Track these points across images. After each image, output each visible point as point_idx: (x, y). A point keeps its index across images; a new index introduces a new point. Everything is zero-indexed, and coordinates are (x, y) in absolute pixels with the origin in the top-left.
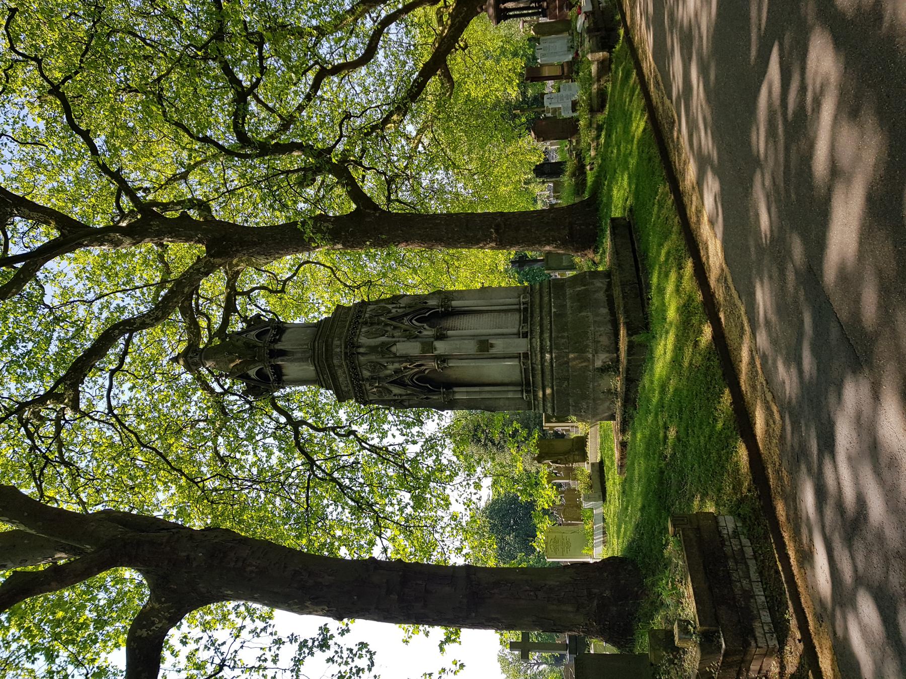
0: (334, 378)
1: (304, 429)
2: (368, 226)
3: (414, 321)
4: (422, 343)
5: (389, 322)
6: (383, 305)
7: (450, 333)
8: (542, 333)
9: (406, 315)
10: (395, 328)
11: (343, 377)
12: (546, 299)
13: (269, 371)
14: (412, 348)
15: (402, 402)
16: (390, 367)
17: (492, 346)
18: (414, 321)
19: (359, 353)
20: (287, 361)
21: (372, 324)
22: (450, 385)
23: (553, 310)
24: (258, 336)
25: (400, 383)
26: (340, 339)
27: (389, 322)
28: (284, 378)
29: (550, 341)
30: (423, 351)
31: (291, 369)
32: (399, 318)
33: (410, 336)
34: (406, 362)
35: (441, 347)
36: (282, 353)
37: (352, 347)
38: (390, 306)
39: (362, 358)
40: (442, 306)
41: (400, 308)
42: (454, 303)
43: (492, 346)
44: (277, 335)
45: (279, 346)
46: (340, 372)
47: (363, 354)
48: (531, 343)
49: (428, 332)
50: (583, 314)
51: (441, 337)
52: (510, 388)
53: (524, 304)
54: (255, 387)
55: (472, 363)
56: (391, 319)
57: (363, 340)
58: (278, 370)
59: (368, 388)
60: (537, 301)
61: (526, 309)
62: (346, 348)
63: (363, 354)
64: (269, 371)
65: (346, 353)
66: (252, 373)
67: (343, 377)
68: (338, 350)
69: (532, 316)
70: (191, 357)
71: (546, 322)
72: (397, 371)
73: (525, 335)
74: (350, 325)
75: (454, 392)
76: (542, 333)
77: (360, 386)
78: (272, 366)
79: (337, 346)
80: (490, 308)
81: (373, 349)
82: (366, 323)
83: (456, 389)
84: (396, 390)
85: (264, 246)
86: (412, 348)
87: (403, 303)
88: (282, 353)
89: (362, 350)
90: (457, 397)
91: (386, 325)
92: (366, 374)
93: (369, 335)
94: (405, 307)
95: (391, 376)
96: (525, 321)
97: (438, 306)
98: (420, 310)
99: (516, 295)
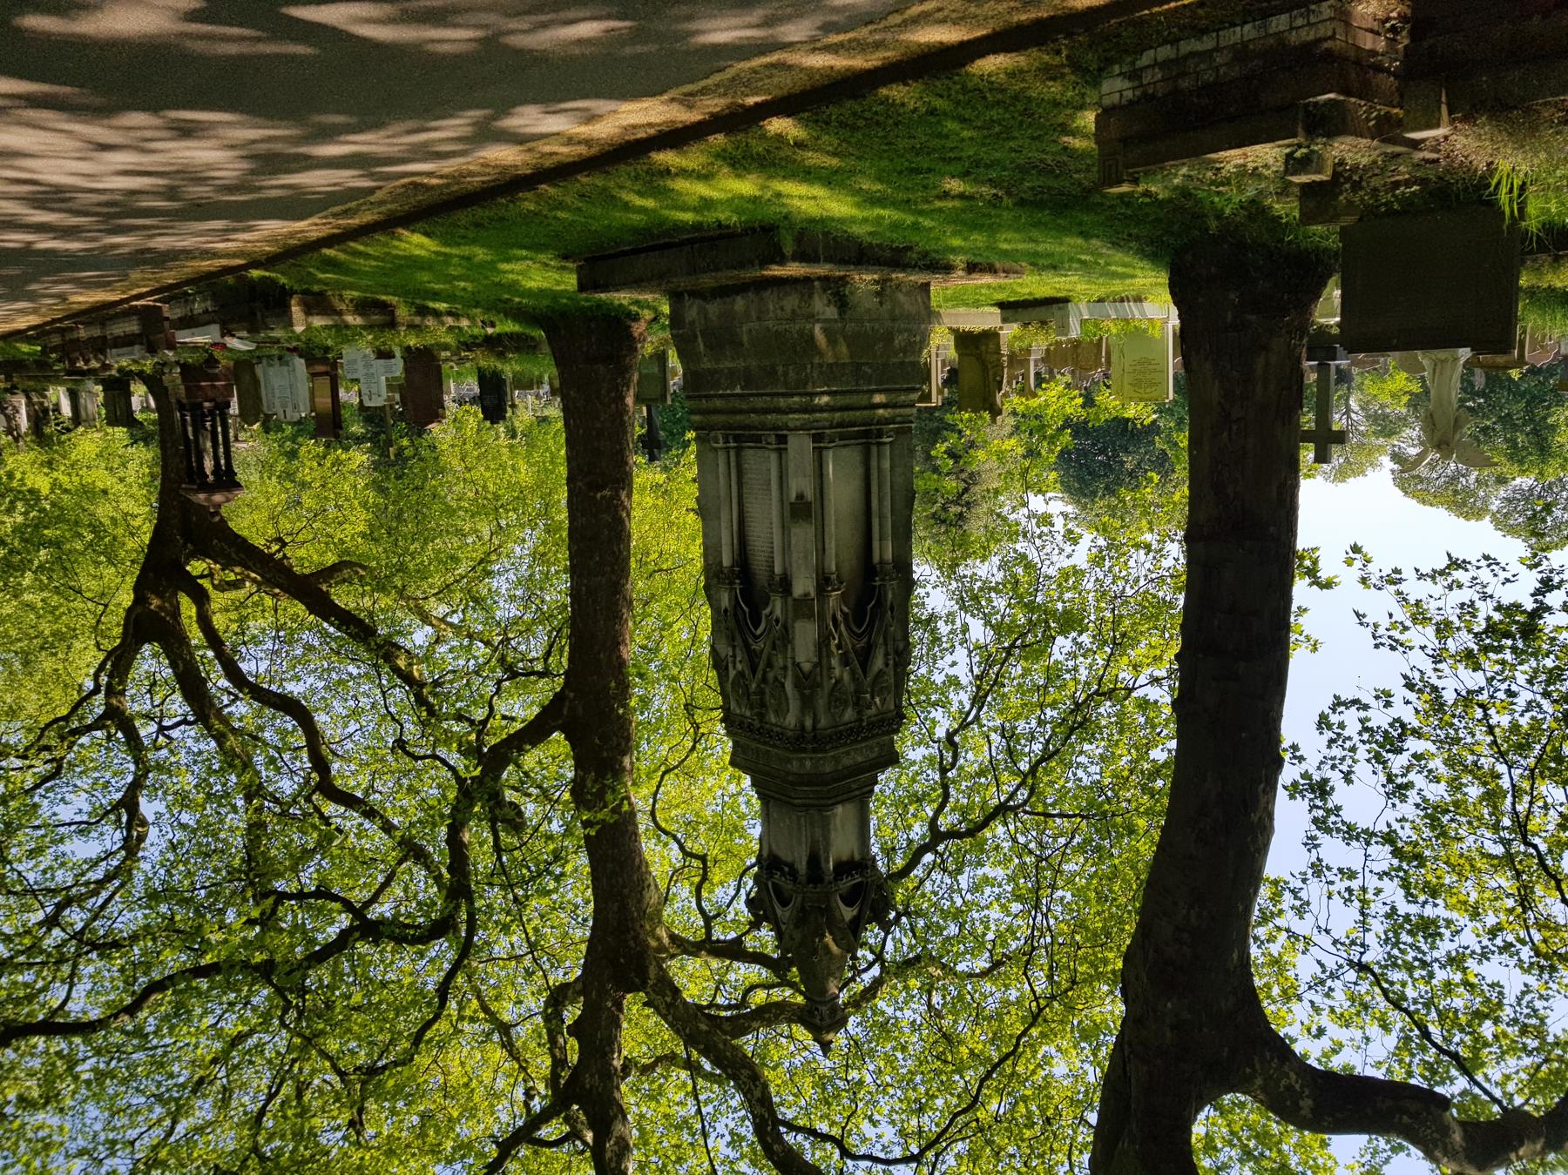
0: (858, 770)
1: (945, 822)
2: (592, 711)
3: (758, 632)
4: (797, 617)
5: (759, 675)
6: (729, 687)
7: (778, 570)
8: (778, 411)
9: (747, 645)
10: (769, 665)
11: (856, 756)
12: (719, 403)
13: (846, 884)
14: (805, 635)
15: (898, 653)
16: (837, 672)
17: (800, 496)
18: (758, 632)
19: (814, 728)
20: (827, 852)
21: (763, 705)
22: (868, 568)
23: (738, 390)
24: (784, 903)
25: (865, 656)
26: (789, 761)
27: (759, 675)
28: (857, 857)
29: (792, 395)
30: (810, 616)
31: (841, 846)
32: (752, 658)
33: (785, 639)
34: (828, 645)
35: (803, 585)
36: (814, 861)
37: (802, 740)
38: (732, 673)
39: (823, 722)
40: (731, 583)
41: (734, 656)
42: (726, 561)
43: (800, 496)
44: (782, 871)
45: (802, 867)
46: (847, 761)
47: (815, 721)
48: (796, 429)
49: (777, 607)
50: (745, 339)
51: (785, 584)
52: (874, 463)
53: (727, 442)
54: (873, 909)
55: (831, 528)
56: (754, 671)
57: (791, 720)
58: (844, 868)
59: (873, 711)
60: (721, 418)
61: (737, 438)
62: (804, 750)
63: (815, 721)
64: (846, 884)
65: (814, 751)
66: (848, 913)
67: (856, 756)
68: (808, 764)
69: (750, 427)
70: (822, 1019)
71: (759, 403)
72: (845, 661)
73: (782, 439)
74: (765, 743)
75: (882, 562)
76: (778, 411)
77: (871, 725)
78: (836, 879)
79: (802, 765)
80: (735, 501)
81: (807, 703)
82: (761, 716)
83: (876, 558)
84: (878, 663)
85: (626, 891)
86: (805, 635)
87: (725, 650)
88: (814, 861)
89: (808, 723)
90: (889, 555)
91: (764, 680)
92: (849, 714)
93: (781, 711)
94: (734, 647)
95: (853, 672)
96: (758, 439)
97: (732, 589)
98: (737, 621)
99: (711, 455)
